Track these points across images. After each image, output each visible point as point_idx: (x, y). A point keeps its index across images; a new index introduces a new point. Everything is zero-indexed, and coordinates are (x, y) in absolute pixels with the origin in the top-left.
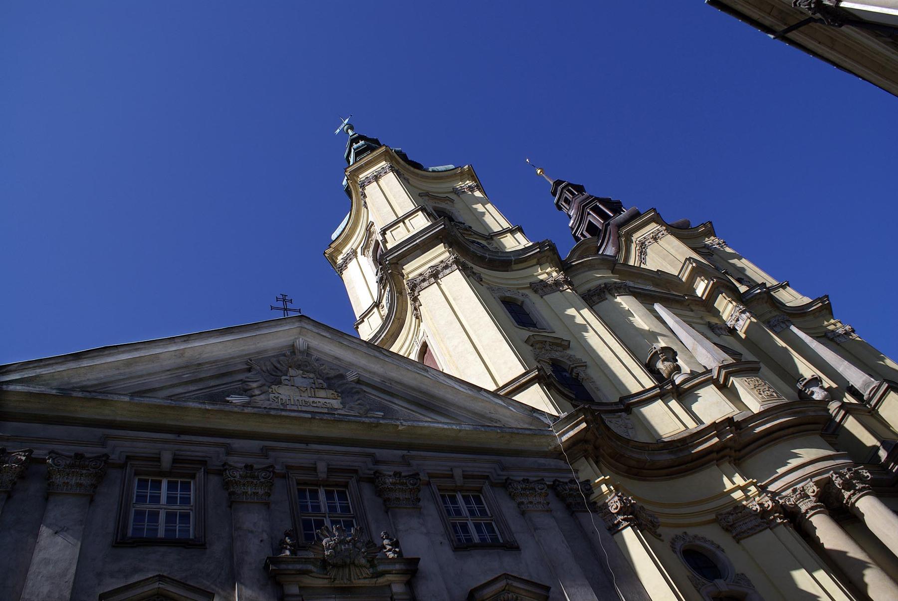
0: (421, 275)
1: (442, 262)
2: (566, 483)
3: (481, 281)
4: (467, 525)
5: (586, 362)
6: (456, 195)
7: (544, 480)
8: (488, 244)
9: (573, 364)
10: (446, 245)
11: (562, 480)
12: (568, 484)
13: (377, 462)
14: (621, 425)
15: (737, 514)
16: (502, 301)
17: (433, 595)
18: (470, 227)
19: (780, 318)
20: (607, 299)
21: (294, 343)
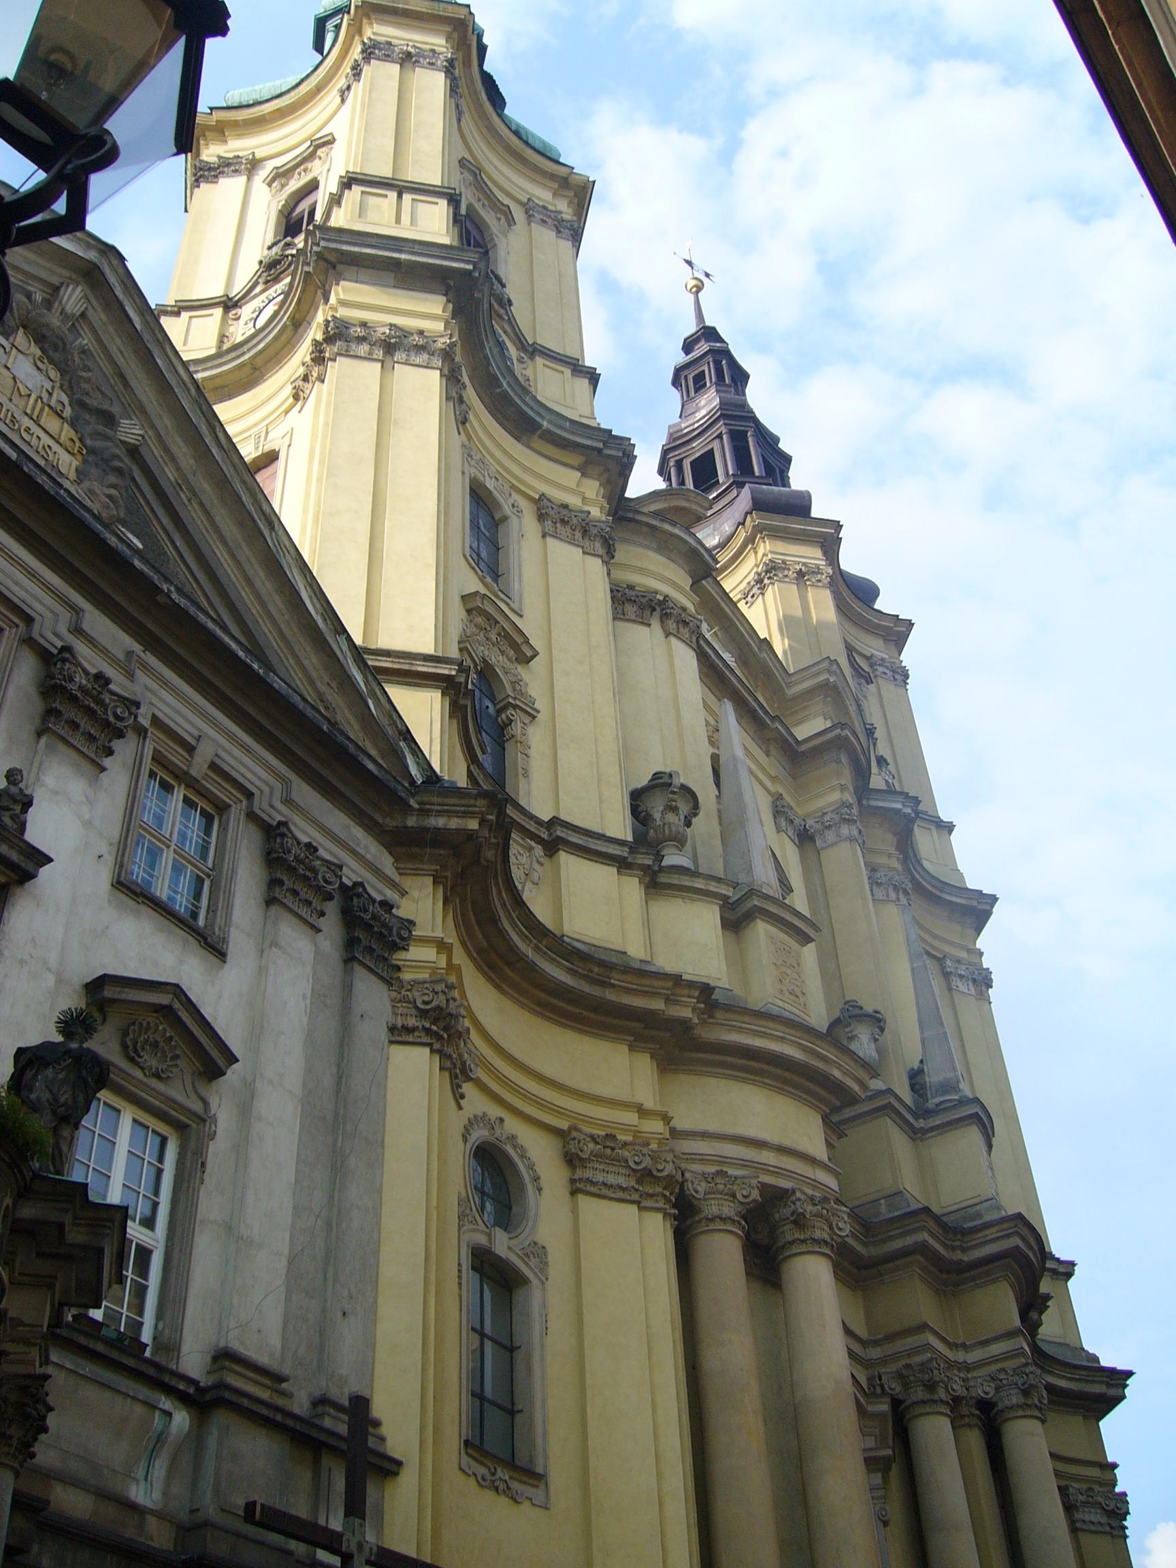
0: (364, 324)
1: (421, 333)
2: (374, 901)
3: (463, 423)
4: (161, 855)
5: (538, 712)
6: (526, 216)
7: (341, 870)
8: (518, 360)
9: (515, 699)
10: (450, 306)
11: (369, 890)
12: (376, 905)
13: (77, 631)
14: (523, 865)
15: (605, 1147)
16: (471, 488)
17: (33, 940)
18: (510, 303)
19: (897, 878)
20: (649, 625)
21: (62, 284)
